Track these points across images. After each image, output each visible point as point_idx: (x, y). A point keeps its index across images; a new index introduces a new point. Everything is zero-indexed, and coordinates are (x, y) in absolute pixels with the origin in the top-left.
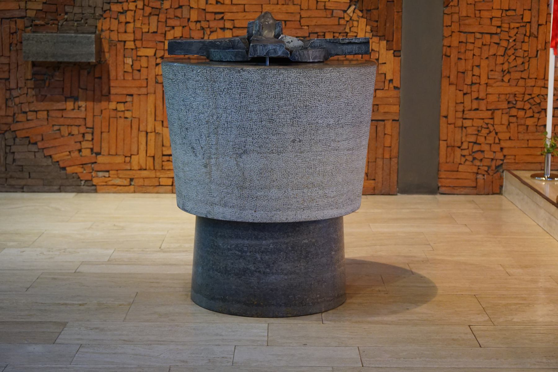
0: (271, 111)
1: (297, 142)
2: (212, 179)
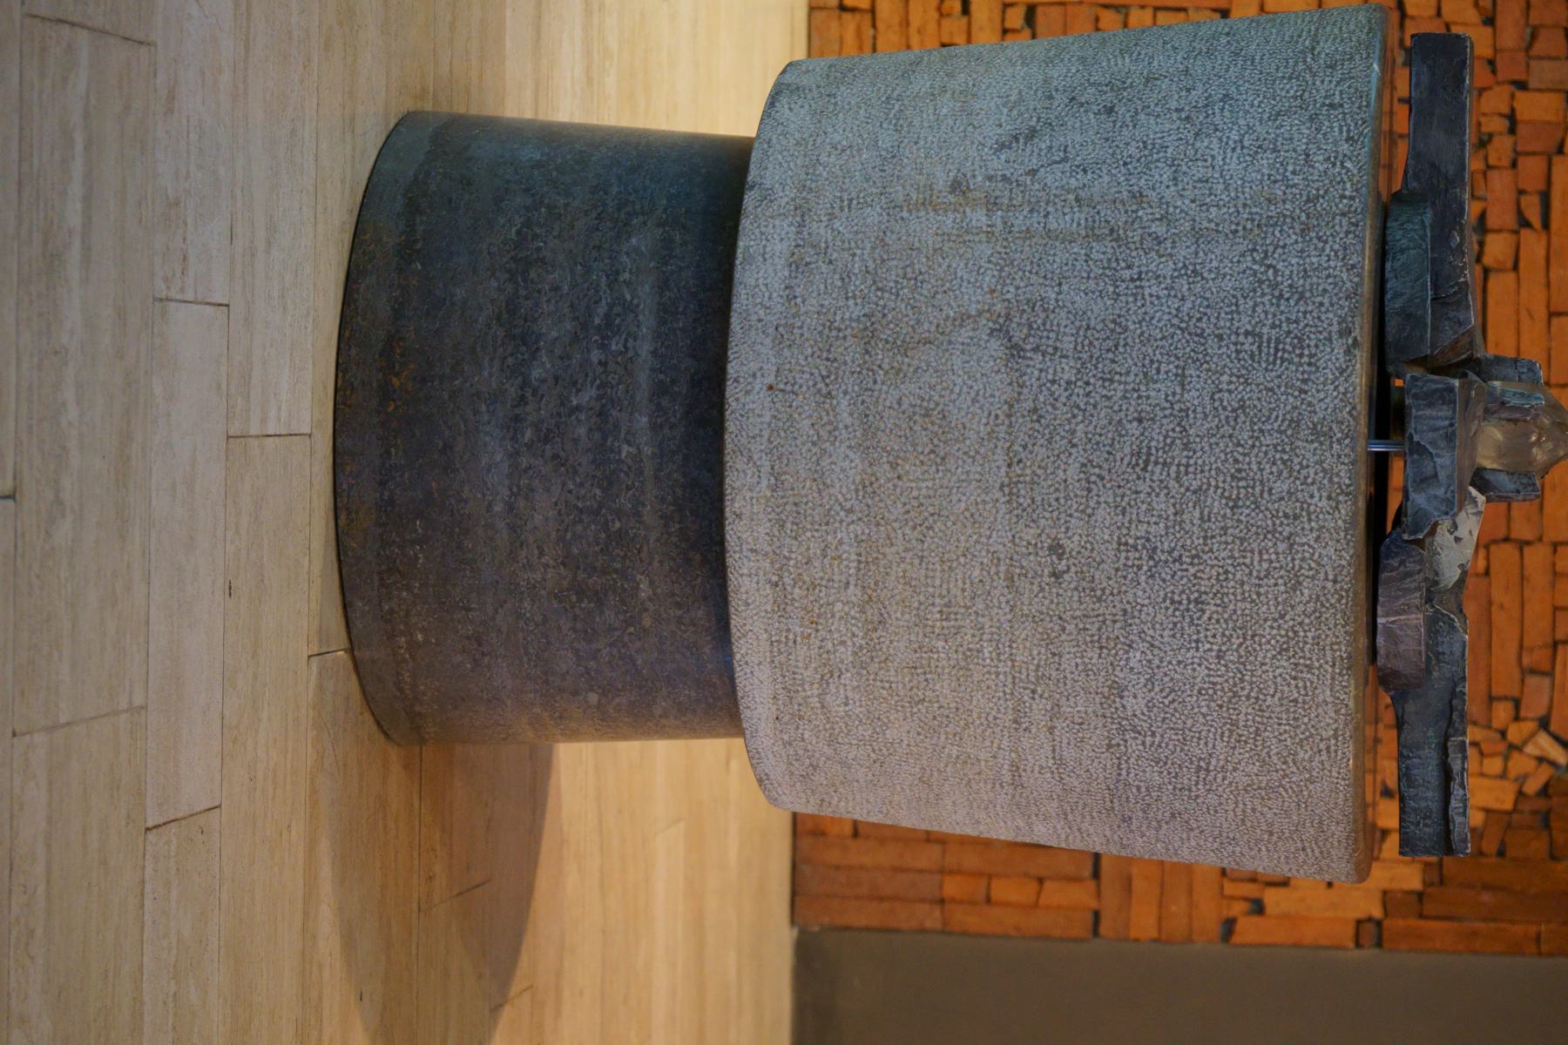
0: (1184, 461)
1: (1052, 563)
2: (905, 214)
